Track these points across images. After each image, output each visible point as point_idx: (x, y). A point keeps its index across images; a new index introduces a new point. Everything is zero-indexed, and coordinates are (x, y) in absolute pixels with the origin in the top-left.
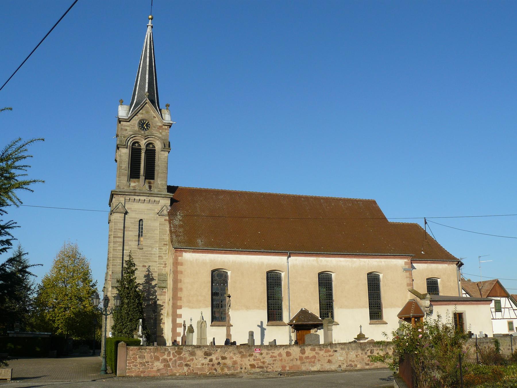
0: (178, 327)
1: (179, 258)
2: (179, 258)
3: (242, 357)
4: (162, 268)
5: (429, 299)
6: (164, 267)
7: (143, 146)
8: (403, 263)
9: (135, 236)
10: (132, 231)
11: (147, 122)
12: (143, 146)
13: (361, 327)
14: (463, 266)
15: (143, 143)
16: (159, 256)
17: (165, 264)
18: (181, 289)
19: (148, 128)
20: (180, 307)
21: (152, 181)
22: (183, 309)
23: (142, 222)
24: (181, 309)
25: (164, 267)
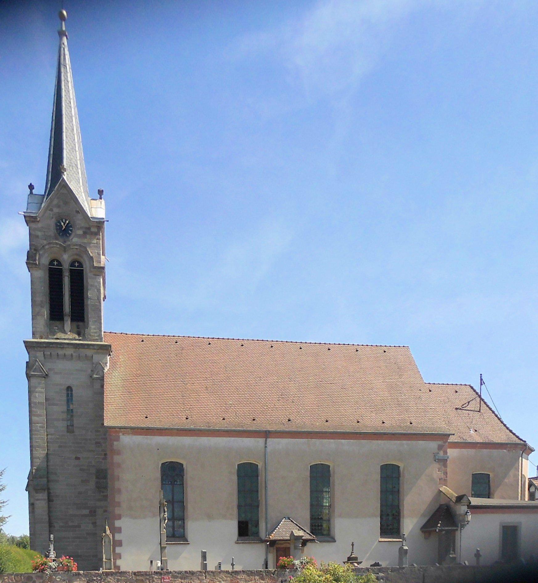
0: (118, 546)
1: (115, 443)
2: (115, 443)
3: (23, 539)
4: (101, 460)
5: (466, 504)
6: (104, 459)
7: (66, 266)
8: (436, 446)
9: (62, 412)
10: (57, 405)
11: (67, 222)
12: (66, 266)
13: (353, 545)
14: (533, 452)
15: (66, 259)
16: (96, 443)
17: (105, 454)
18: (119, 491)
19: (59, 224)
20: (119, 517)
21: (81, 324)
22: (123, 519)
23: (72, 390)
24: (121, 519)
25: (104, 459)
